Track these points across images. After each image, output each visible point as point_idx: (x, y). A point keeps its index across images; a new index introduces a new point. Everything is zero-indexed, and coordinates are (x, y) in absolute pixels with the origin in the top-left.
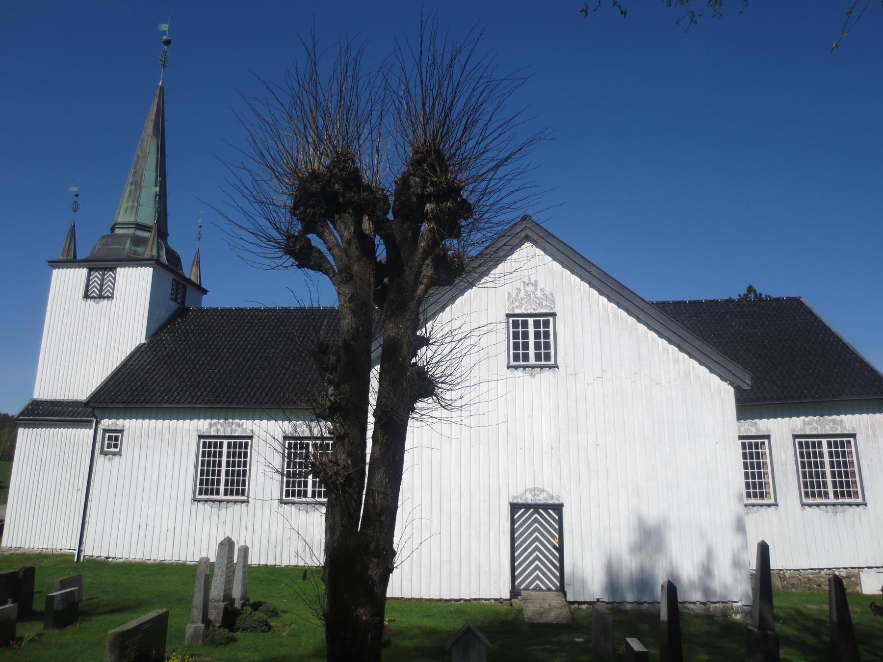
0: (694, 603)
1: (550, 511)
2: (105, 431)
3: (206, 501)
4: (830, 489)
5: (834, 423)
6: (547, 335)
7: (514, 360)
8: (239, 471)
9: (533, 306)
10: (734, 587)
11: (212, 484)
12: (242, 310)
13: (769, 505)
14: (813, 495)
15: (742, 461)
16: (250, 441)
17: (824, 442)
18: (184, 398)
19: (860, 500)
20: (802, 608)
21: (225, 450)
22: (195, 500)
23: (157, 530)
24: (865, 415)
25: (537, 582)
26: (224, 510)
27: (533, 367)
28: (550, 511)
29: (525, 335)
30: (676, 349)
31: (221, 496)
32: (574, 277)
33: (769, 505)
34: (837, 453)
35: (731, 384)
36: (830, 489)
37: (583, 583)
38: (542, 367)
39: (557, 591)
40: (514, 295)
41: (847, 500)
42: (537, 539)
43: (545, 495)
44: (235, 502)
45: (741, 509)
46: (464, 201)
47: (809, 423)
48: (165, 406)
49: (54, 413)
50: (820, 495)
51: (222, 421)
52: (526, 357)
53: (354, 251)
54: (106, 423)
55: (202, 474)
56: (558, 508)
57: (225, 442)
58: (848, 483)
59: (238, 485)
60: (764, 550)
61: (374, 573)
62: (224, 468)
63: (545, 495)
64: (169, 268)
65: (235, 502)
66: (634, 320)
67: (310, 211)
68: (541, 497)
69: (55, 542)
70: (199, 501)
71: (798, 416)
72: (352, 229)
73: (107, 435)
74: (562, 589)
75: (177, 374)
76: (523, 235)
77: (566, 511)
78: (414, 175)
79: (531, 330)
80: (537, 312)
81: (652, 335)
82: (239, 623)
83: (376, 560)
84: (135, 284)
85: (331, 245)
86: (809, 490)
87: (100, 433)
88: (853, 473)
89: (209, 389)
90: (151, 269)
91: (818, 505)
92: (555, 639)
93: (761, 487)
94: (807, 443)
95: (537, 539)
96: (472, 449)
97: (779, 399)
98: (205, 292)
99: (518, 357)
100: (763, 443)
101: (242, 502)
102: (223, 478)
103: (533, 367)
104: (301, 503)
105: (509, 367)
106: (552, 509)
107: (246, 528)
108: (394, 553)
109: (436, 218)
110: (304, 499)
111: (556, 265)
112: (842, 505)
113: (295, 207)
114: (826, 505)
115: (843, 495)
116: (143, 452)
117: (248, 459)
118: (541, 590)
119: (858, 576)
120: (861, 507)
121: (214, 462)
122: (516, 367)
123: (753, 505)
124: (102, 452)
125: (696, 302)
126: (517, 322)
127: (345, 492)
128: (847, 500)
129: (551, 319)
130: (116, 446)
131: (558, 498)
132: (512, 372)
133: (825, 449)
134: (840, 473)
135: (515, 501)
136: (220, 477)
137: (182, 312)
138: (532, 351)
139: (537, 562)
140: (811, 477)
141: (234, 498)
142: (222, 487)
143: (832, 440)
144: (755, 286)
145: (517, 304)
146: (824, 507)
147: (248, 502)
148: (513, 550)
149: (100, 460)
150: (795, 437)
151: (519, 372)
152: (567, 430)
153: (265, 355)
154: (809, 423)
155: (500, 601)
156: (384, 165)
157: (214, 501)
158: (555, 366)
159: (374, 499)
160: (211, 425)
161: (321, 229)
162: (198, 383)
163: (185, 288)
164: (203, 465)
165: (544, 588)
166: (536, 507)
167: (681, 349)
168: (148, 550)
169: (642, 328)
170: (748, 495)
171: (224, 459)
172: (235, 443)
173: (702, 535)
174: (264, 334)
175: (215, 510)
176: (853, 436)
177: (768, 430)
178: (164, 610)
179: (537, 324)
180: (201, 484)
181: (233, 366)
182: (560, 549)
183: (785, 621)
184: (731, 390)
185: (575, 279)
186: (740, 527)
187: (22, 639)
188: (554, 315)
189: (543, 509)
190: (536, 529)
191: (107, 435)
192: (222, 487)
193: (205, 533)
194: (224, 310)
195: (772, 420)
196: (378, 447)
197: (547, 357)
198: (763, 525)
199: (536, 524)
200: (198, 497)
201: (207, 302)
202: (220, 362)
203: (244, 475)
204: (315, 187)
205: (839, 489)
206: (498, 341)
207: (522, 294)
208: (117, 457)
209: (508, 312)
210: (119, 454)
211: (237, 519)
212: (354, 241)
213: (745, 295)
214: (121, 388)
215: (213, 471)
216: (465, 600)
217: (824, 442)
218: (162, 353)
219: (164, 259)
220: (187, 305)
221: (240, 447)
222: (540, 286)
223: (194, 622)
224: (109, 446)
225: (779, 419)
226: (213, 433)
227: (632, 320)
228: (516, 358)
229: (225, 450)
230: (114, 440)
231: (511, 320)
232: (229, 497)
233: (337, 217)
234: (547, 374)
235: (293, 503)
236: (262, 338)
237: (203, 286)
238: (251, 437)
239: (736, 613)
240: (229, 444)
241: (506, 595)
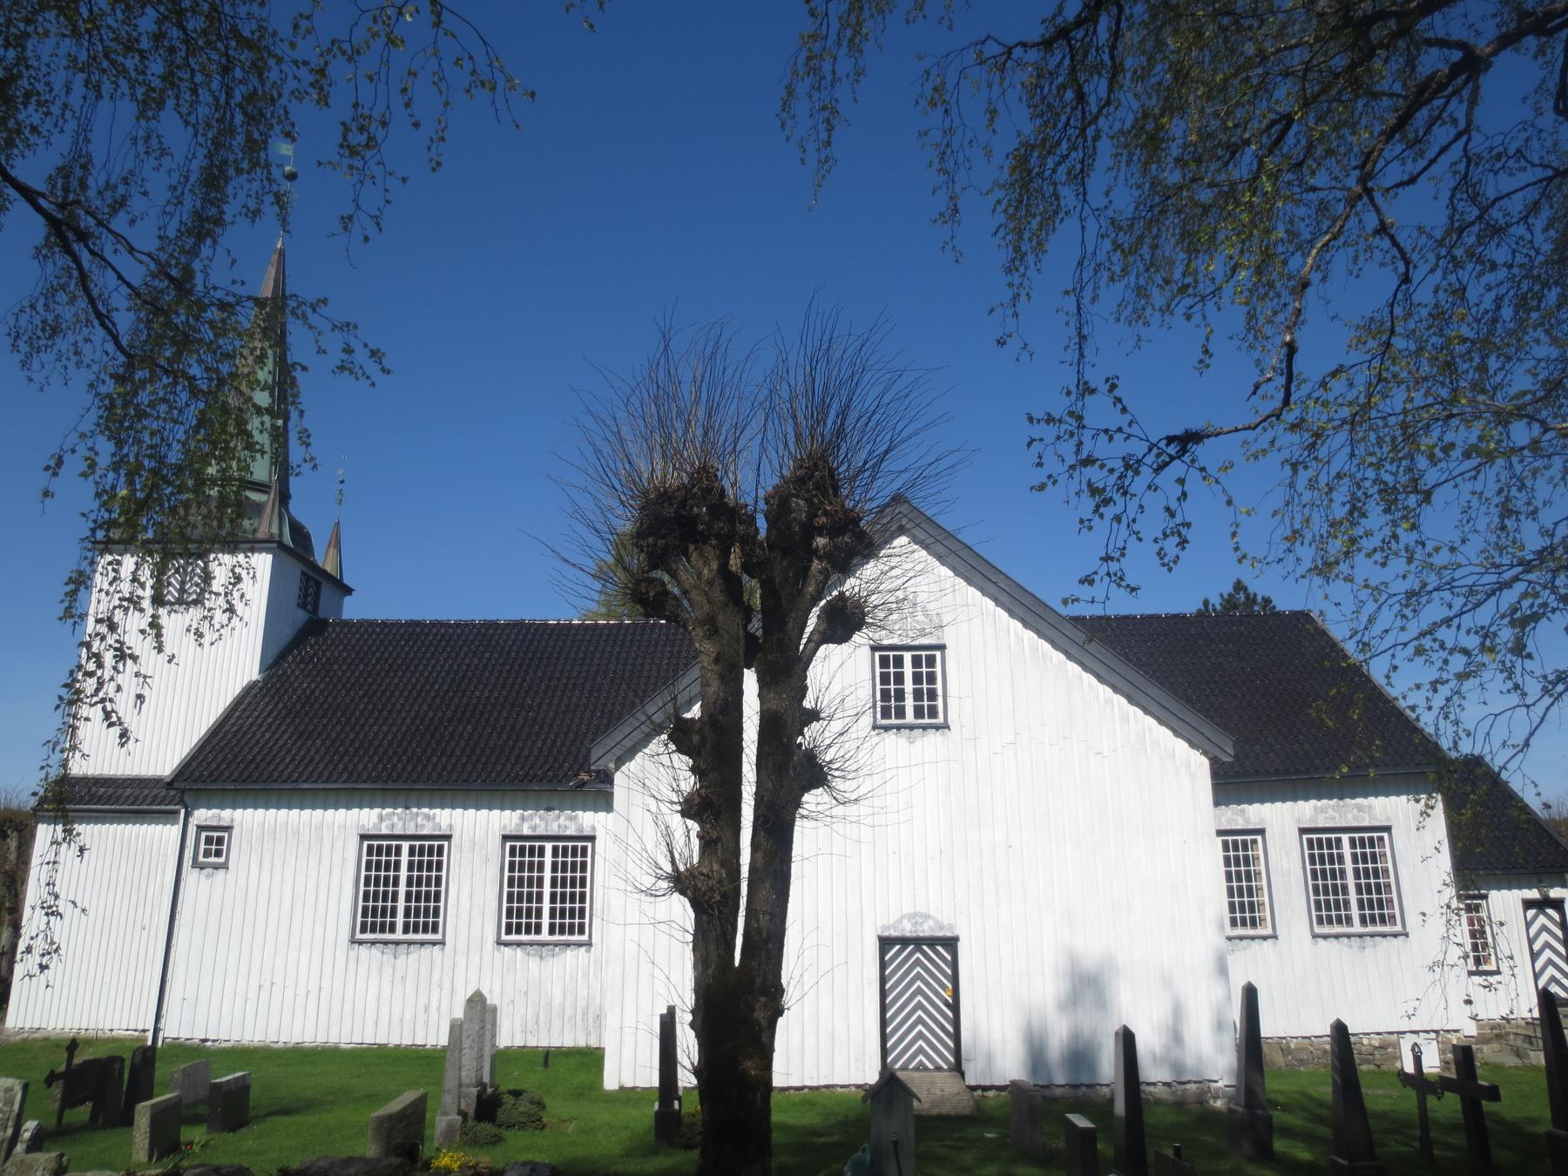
0: (1154, 1084)
2: (200, 828)
3: (373, 943)
4: (1355, 912)
6: (932, 678)
8: (428, 894)
10: (1214, 1060)
11: (384, 915)
12: (417, 624)
13: (1265, 938)
14: (1330, 921)
15: (1223, 869)
16: (446, 844)
17: (1345, 838)
18: (336, 774)
19: (1398, 928)
20: (1312, 1092)
21: (405, 858)
22: (354, 941)
23: (289, 993)
25: (921, 1057)
26: (403, 957)
27: (911, 728)
29: (899, 678)
30: (1123, 701)
31: (399, 935)
32: (972, 590)
33: (1265, 938)
34: (1364, 855)
35: (1205, 753)
36: (1355, 912)
37: (989, 1058)
38: (925, 728)
39: (950, 1070)
44: (422, 943)
45: (1223, 942)
46: (863, 533)
47: (1323, 810)
48: (306, 786)
49: (101, 798)
50: (1339, 921)
51: (399, 810)
52: (901, 713)
53: (718, 595)
54: (202, 815)
55: (366, 899)
56: (951, 943)
57: (405, 846)
58: (1380, 901)
59: (426, 915)
60: (1250, 994)
61: (760, 1015)
62: (402, 889)
63: (931, 923)
64: (295, 549)
65: (422, 943)
66: (1062, 657)
67: (661, 542)
68: (926, 927)
69: (101, 1016)
70: (361, 943)
71: (1307, 799)
72: (715, 565)
73: (204, 835)
74: (958, 1068)
75: (320, 734)
77: (962, 947)
78: (797, 496)
79: (908, 670)
81: (1089, 679)
82: (501, 1115)
83: (763, 999)
84: (250, 581)
85: (687, 587)
87: (192, 830)
88: (1388, 886)
89: (376, 758)
90: (270, 557)
91: (1337, 936)
92: (957, 1135)
93: (1252, 910)
94: (1320, 841)
97: (1277, 772)
98: (348, 591)
100: (1254, 842)
101: (434, 944)
102: (401, 904)
103: (911, 728)
104: (531, 944)
107: (440, 986)
108: (783, 991)
109: (829, 556)
112: (1372, 935)
113: (639, 535)
114: (1349, 936)
115: (1373, 921)
116: (267, 865)
117: (444, 873)
118: (926, 1069)
120: (1401, 939)
121: (387, 878)
122: (887, 728)
123: (1241, 938)
124: (196, 864)
125: (1150, 617)
127: (720, 912)
129: (938, 654)
130: (218, 853)
131: (951, 927)
133: (1347, 850)
134: (1368, 886)
135: (886, 934)
136: (400, 901)
137: (315, 627)
138: (909, 703)
140: (1326, 893)
141: (420, 936)
142: (400, 920)
144: (1246, 581)
147: (442, 943)
149: (191, 877)
150: (1303, 831)
151: (891, 737)
152: (1017, 837)
153: (465, 700)
154: (1323, 810)
156: (752, 479)
157: (386, 943)
159: (758, 921)
160: (381, 818)
161: (674, 566)
162: (357, 750)
163: (318, 584)
164: (367, 883)
166: (918, 942)
167: (1131, 701)
168: (274, 1024)
169: (1074, 668)
170: (1234, 923)
171: (404, 873)
172: (522, 848)
173: (1167, 981)
174: (459, 666)
175: (388, 957)
177: (1262, 820)
178: (422, 1091)
179: (916, 662)
180: (364, 915)
181: (414, 719)
182: (955, 1007)
183: (1286, 1108)
184: (1206, 762)
186: (1222, 970)
187: (191, 1143)
188: (942, 648)
191: (204, 835)
192: (400, 920)
193: (372, 996)
194: (384, 624)
195: (1268, 805)
196: (759, 855)
197: (933, 712)
198: (1254, 963)
200: (359, 936)
201: (353, 609)
202: (390, 712)
203: (437, 899)
204: (669, 511)
205: (1367, 912)
208: (221, 872)
210: (225, 866)
211: (424, 971)
212: (718, 582)
213: (1230, 595)
214: (226, 757)
215: (385, 893)
216: (811, 1088)
217: (1345, 838)
218: (290, 698)
219: (287, 539)
220: (322, 614)
221: (574, 855)
223: (445, 1113)
224: (207, 854)
225: (1278, 804)
226: (384, 831)
227: (1058, 656)
228: (886, 713)
230: (216, 844)
231: (877, 654)
232: (411, 936)
233: (692, 547)
234: (932, 737)
235: (519, 944)
236: (456, 672)
237: (346, 581)
238: (448, 838)
239: (1216, 1098)
240: (412, 849)
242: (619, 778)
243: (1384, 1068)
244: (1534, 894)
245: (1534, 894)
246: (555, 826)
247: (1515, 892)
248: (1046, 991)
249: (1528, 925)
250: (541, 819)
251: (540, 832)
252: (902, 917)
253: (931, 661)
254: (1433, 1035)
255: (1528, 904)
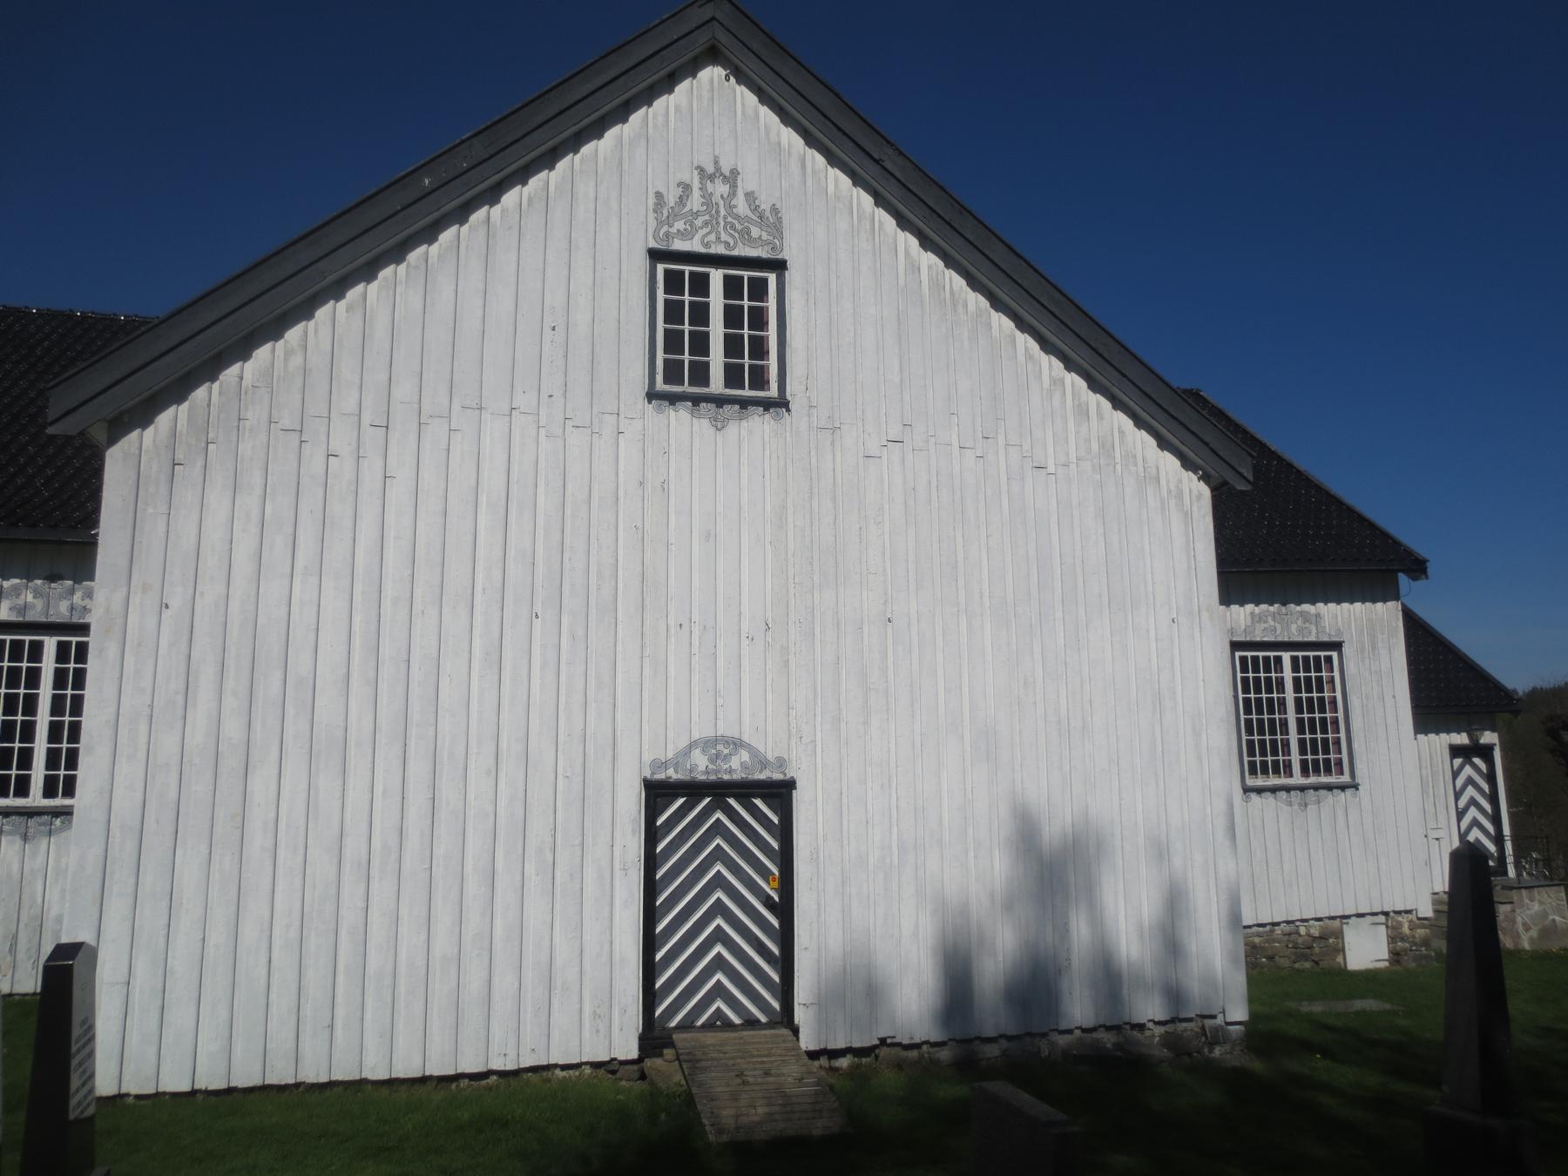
1: (758, 802)
5: (1306, 620)
7: (667, 381)
9: (724, 237)
17: (1286, 657)
19: (1346, 778)
24: (1358, 605)
25: (719, 1004)
27: (720, 401)
28: (758, 802)
35: (1206, 478)
38: (744, 403)
39: (771, 1025)
40: (671, 200)
41: (1324, 779)
42: (719, 881)
43: (745, 756)
50: (1276, 771)
56: (780, 793)
63: (745, 756)
66: (984, 302)
68: (735, 763)
76: (702, 40)
80: (735, 253)
86: (1258, 759)
91: (1274, 790)
95: (719, 881)
96: (537, 623)
99: (678, 377)
103: (720, 401)
105: (652, 396)
106: (764, 798)
110: (20, 802)
111: (790, 138)
112: (1316, 788)
118: (728, 1025)
119: (1339, 935)
120: (1349, 792)
122: (673, 399)
126: (677, 273)
128: (1324, 779)
131: (781, 763)
132: (659, 410)
135: (661, 776)
139: (719, 948)
143: (1300, 654)
145: (679, 225)
146: (1283, 794)
148: (651, 914)
151: (680, 416)
155: (609, 1067)
158: (782, 403)
165: (737, 1020)
166: (719, 791)
167: (1094, 385)
173: (1160, 851)
176: (1337, 646)
179: (700, 374)
182: (784, 908)
185: (838, 180)
188: (779, 266)
189: (737, 797)
190: (718, 854)
197: (759, 379)
199: (718, 841)
206: (625, 310)
207: (695, 202)
209: (653, 244)
216: (503, 1074)
217: (1286, 657)
222: (746, 183)
228: (673, 372)
229: (1288, 674)
231: (660, 268)
234: (758, 425)
241: (627, 1048)
242: (117, 463)
243: (1324, 964)
244: (1462, 739)
245: (1462, 739)
246: (63, 607)
247: (1443, 736)
248: (980, 872)
249: (1455, 775)
250: (37, 594)
251: (35, 615)
252: (692, 746)
253: (759, 289)
254: (1382, 919)
255: (1456, 751)
